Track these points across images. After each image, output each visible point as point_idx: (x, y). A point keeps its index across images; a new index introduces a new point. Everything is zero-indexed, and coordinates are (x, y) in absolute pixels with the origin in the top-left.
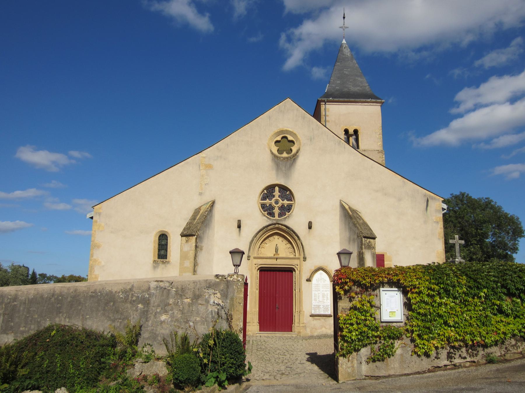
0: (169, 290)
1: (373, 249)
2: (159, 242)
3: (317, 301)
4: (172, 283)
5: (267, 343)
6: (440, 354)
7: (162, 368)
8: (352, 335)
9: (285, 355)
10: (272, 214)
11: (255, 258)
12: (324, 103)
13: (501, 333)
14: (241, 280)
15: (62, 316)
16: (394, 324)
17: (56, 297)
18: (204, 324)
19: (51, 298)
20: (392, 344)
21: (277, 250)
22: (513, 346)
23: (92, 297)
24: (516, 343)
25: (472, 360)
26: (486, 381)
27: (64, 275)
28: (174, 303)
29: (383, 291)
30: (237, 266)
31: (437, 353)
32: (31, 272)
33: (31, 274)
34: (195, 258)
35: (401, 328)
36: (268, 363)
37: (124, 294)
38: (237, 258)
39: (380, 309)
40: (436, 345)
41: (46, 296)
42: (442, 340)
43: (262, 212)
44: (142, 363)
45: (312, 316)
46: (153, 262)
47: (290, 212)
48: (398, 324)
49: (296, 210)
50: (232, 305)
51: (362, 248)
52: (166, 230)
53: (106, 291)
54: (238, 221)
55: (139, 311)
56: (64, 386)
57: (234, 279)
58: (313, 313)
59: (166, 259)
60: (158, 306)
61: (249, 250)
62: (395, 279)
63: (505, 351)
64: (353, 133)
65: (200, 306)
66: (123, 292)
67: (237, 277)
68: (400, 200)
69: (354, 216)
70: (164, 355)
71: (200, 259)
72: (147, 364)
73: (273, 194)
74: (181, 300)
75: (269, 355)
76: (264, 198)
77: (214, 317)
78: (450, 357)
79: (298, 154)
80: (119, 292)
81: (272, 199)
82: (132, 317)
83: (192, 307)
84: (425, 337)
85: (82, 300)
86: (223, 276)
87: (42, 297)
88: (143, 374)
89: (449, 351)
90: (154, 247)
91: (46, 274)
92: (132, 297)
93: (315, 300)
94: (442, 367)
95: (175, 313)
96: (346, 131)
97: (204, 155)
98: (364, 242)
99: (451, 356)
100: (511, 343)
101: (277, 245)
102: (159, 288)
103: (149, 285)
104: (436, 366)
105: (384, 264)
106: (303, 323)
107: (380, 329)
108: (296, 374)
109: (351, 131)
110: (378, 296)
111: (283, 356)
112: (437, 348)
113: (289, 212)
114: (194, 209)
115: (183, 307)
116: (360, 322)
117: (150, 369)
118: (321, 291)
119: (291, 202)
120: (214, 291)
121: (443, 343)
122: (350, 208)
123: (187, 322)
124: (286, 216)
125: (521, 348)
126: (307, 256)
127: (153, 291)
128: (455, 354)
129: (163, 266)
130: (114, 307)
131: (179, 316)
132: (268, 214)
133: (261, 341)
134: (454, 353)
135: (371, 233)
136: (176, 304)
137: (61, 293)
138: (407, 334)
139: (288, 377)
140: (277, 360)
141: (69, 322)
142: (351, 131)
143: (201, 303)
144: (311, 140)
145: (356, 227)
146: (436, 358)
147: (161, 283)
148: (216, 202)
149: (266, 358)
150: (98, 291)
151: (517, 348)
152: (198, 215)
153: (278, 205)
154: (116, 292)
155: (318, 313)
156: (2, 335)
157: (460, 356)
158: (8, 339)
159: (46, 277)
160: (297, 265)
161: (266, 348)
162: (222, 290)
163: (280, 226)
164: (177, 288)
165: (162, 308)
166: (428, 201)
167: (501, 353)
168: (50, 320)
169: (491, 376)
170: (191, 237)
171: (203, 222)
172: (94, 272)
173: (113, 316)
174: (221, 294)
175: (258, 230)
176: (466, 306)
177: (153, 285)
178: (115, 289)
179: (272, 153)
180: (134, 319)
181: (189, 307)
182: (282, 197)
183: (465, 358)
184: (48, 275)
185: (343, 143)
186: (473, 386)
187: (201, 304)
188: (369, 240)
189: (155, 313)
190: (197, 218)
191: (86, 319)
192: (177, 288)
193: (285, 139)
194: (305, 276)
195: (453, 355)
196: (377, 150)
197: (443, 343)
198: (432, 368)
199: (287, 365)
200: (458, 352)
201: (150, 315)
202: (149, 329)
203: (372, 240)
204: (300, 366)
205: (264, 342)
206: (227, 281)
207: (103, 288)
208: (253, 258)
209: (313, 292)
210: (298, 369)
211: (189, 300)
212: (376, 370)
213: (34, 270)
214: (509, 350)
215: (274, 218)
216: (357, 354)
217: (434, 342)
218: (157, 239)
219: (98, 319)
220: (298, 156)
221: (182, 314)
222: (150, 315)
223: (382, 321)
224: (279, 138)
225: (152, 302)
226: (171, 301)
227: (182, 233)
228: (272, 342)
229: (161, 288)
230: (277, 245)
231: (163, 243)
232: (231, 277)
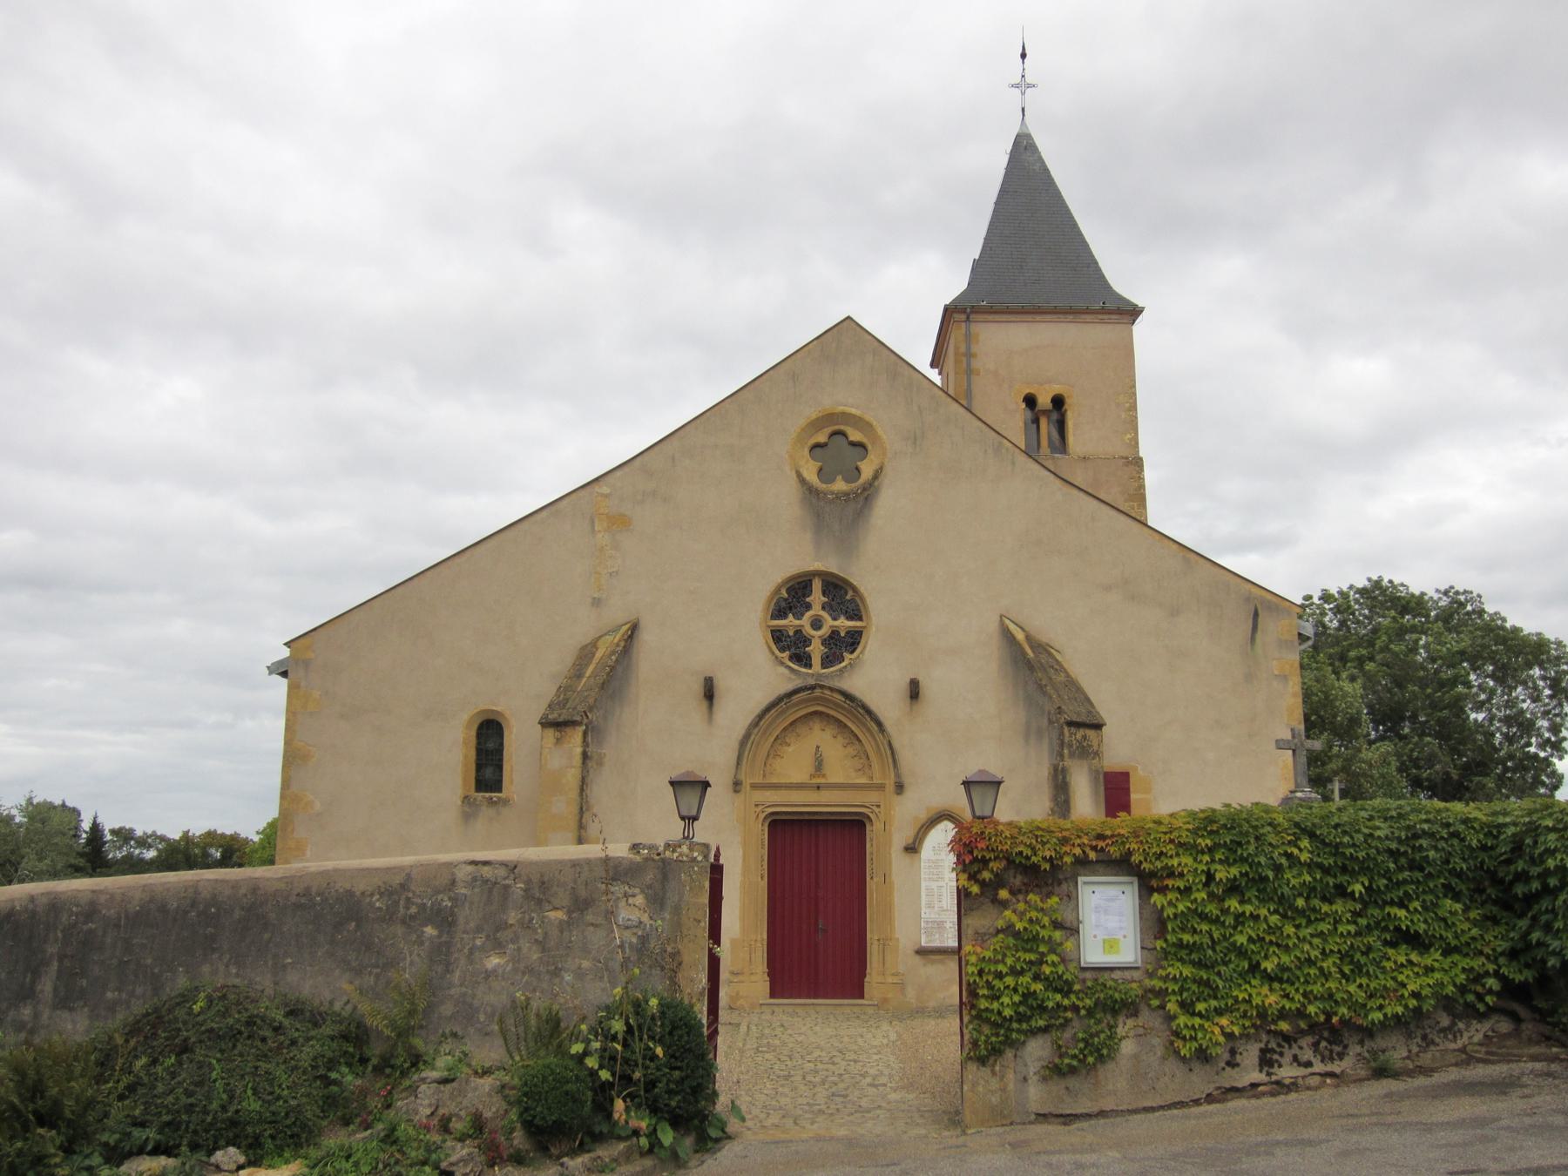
0: (506, 887)
1: (1093, 759)
2: (479, 743)
3: (936, 909)
4: (516, 867)
5: (789, 1032)
6: (1241, 1054)
7: (489, 1095)
8: (1002, 1003)
9: (833, 1063)
10: (802, 659)
11: (754, 786)
12: (963, 317)
13: (1406, 994)
14: (700, 858)
15: (220, 958)
16: (1117, 975)
17: (201, 907)
18: (601, 978)
19: (187, 912)
20: (1110, 1027)
21: (819, 765)
22: (1443, 1030)
23: (298, 906)
24: (1454, 1024)
25: (1330, 1068)
26: (1344, 1121)
27: (188, 831)
28: (521, 923)
29: (1085, 883)
30: (689, 819)
31: (1233, 1052)
32: (86, 825)
33: (88, 829)
34: (582, 790)
35: (1134, 985)
36: (782, 1086)
37: (386, 898)
38: (691, 798)
39: (1078, 932)
40: (1228, 1030)
41: (175, 904)
42: (1244, 1016)
43: (773, 653)
44: (435, 1085)
45: (922, 952)
46: (463, 802)
47: (855, 654)
48: (1127, 975)
49: (871, 646)
50: (677, 926)
51: (1062, 756)
52: (499, 709)
53: (337, 891)
54: (705, 679)
55: (427, 944)
56: (234, 1145)
57: (681, 855)
58: (923, 944)
59: (499, 790)
60: (479, 929)
61: (738, 764)
62: (1115, 852)
63: (1419, 1046)
64: (1049, 406)
65: (591, 928)
66: (381, 894)
67: (691, 849)
68: (1174, 612)
69: (1039, 662)
70: (495, 1063)
71: (598, 791)
72: (449, 1086)
73: (808, 600)
74: (538, 916)
75: (789, 1063)
76: (779, 613)
77: (629, 958)
78: (1266, 1061)
79: (876, 483)
80: (372, 895)
81: (803, 615)
82: (408, 959)
83: (570, 931)
84: (1201, 1007)
85: (272, 916)
86: (651, 847)
87: (163, 908)
88: (441, 1111)
89: (1266, 1045)
90: (466, 757)
91: (131, 831)
92: (408, 908)
93: (930, 906)
94: (1244, 1088)
95: (525, 950)
96: (1030, 401)
97: (605, 488)
98: (1067, 739)
99: (1271, 1059)
100: (1438, 1023)
101: (818, 747)
102: (478, 883)
103: (453, 874)
104: (1227, 1086)
105: (1129, 801)
106: (896, 974)
107: (1077, 987)
108: (856, 1112)
109: (1044, 401)
110: (1071, 898)
111: (826, 1066)
112: (1230, 1036)
113: (852, 652)
114: (579, 647)
115: (546, 933)
116: (1022, 968)
117: (459, 1099)
118: (947, 881)
119: (858, 624)
120: (627, 888)
121: (1247, 1024)
122: (1028, 638)
123: (556, 973)
124: (843, 664)
125: (1466, 1035)
126: (907, 780)
127: (463, 891)
128: (1281, 1054)
129: (491, 812)
130: (359, 934)
131: (535, 957)
132: (791, 659)
133: (774, 1025)
134: (1278, 1050)
135: (1090, 712)
136: (527, 925)
137: (214, 896)
138: (1150, 999)
139: (832, 1121)
140: (809, 1078)
141: (237, 975)
142: (1044, 401)
143: (594, 922)
144: (915, 443)
145: (1045, 693)
146: (1228, 1064)
147: (486, 868)
148: (642, 624)
149: (779, 1072)
150: (314, 890)
151: (1455, 1037)
152: (587, 665)
153: (820, 633)
154: (363, 893)
155: (937, 944)
156: (58, 1012)
157: (1295, 1058)
158: (74, 1022)
159: (132, 838)
160: (878, 806)
161: (784, 1044)
162: (650, 887)
163: (826, 692)
164: (529, 882)
165: (488, 937)
166: (1256, 615)
167: (1410, 1051)
168: (187, 972)
169: (1365, 1111)
170: (568, 730)
171: (603, 683)
172: (293, 831)
173: (357, 959)
174: (647, 898)
175: (757, 711)
176: (1309, 922)
177: (463, 873)
178: (360, 886)
179: (802, 480)
180: (412, 966)
181: (562, 932)
182: (831, 607)
183: (1309, 1064)
184: (139, 833)
185: (1007, 449)
186: (1306, 1136)
187: (592, 924)
188: (1080, 733)
189: (471, 949)
190: (587, 675)
191: (284, 966)
192: (529, 882)
193: (839, 438)
194: (900, 838)
195: (1276, 1057)
196: (1122, 458)
197: (1247, 1024)
198: (1219, 1092)
199: (834, 1089)
200: (1290, 1047)
201: (456, 955)
202: (453, 991)
203: (1091, 733)
204: (872, 1091)
205: (782, 1029)
206: (663, 861)
207: (328, 884)
208: (748, 787)
209: (923, 885)
210: (865, 1099)
211: (560, 915)
212: (1064, 1097)
213: (95, 818)
214: (1433, 1042)
215: (810, 671)
216: (1015, 1056)
217: (1224, 1021)
218: (473, 733)
219: (317, 968)
220: (877, 490)
221: (544, 950)
222: (456, 955)
223: (1083, 965)
224: (822, 438)
225: (461, 920)
226: (513, 917)
227: (545, 716)
228: (804, 1029)
229: (486, 881)
230: (818, 747)
231: (491, 745)
232: (674, 851)
